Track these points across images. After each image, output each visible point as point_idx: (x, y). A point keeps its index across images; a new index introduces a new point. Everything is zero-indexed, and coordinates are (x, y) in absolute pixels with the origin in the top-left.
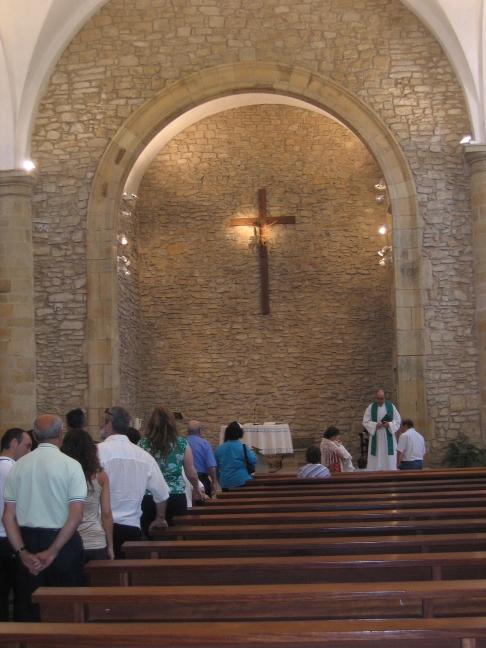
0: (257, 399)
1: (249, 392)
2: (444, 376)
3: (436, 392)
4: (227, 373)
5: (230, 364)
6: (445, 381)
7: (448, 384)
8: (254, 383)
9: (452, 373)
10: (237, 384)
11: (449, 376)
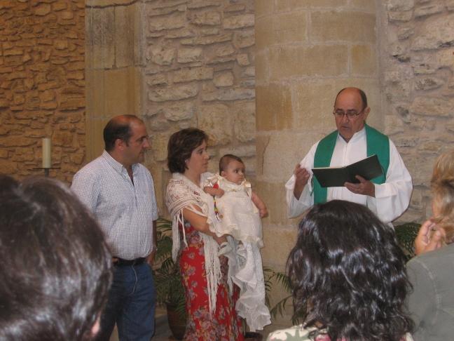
0: (60, 118)
1: (52, 105)
2: (188, 54)
3: (168, 96)
4: (22, 75)
5: (26, 58)
6: (188, 66)
7: (193, 74)
8: (59, 91)
9: (205, 47)
10: (36, 94)
11: (197, 52)
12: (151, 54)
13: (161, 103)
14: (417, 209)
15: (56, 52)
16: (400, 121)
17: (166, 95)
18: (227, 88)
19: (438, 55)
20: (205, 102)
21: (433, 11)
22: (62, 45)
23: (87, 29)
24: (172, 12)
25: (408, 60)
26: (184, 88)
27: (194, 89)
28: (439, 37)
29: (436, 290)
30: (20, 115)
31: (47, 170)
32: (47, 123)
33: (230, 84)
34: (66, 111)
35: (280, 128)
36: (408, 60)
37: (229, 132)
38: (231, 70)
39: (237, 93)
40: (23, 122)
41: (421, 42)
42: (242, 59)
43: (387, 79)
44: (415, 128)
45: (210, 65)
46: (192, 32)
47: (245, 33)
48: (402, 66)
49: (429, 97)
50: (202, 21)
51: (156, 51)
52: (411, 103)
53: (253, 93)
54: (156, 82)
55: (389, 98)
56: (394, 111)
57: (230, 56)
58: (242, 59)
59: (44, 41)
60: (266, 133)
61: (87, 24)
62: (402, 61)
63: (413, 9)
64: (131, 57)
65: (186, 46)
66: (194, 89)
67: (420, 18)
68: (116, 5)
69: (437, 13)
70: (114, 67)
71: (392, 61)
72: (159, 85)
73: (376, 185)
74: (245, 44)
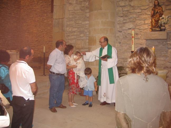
4: (41, 34)
5: (42, 30)
6: (74, 32)
7: (75, 34)
11: (76, 29)
12: (67, 29)
13: (69, 39)
14: (122, 63)
15: (48, 30)
16: (119, 45)
17: (70, 38)
18: (82, 37)
19: (128, 31)
20: (78, 40)
21: (127, 21)
22: (49, 28)
23: (53, 24)
24: (71, 21)
25: (121, 32)
26: (73, 36)
27: (76, 37)
28: (128, 27)
29: (122, 87)
30: (40, 42)
31: (44, 53)
32: (46, 44)
33: (83, 36)
34: (50, 41)
35: (94, 45)
36: (121, 32)
37: (83, 46)
38: (83, 33)
39: (85, 38)
40: (41, 44)
41: (124, 28)
42: (86, 31)
43: (116, 36)
44: (122, 46)
45: (79, 32)
46: (75, 25)
47: (87, 25)
48: (120, 33)
49: (125, 40)
50: (78, 22)
51: (68, 29)
52: (121, 41)
53: (88, 38)
54: (68, 35)
55: (117, 40)
56: (118, 43)
57: (83, 30)
58: (86, 31)
59: (45, 27)
60: (90, 46)
61: (54, 23)
62: (120, 32)
63: (123, 21)
64: (63, 30)
65: (74, 28)
66: (76, 37)
67: (124, 23)
68: (60, 19)
69: (128, 22)
70: (59, 32)
71: (118, 32)
72: (68, 36)
73: (13, 95)
74: (87, 28)
